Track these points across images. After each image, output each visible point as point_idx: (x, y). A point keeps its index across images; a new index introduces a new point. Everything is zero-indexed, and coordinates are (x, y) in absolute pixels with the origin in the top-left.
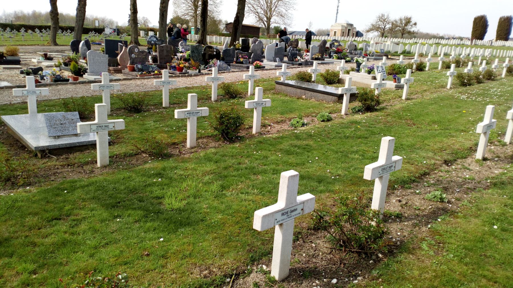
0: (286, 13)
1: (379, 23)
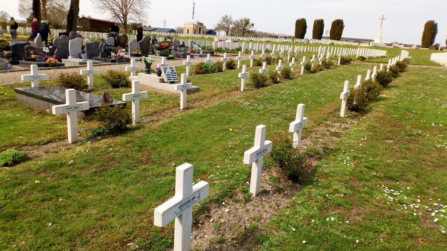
0: (141, 10)
1: (224, 23)
